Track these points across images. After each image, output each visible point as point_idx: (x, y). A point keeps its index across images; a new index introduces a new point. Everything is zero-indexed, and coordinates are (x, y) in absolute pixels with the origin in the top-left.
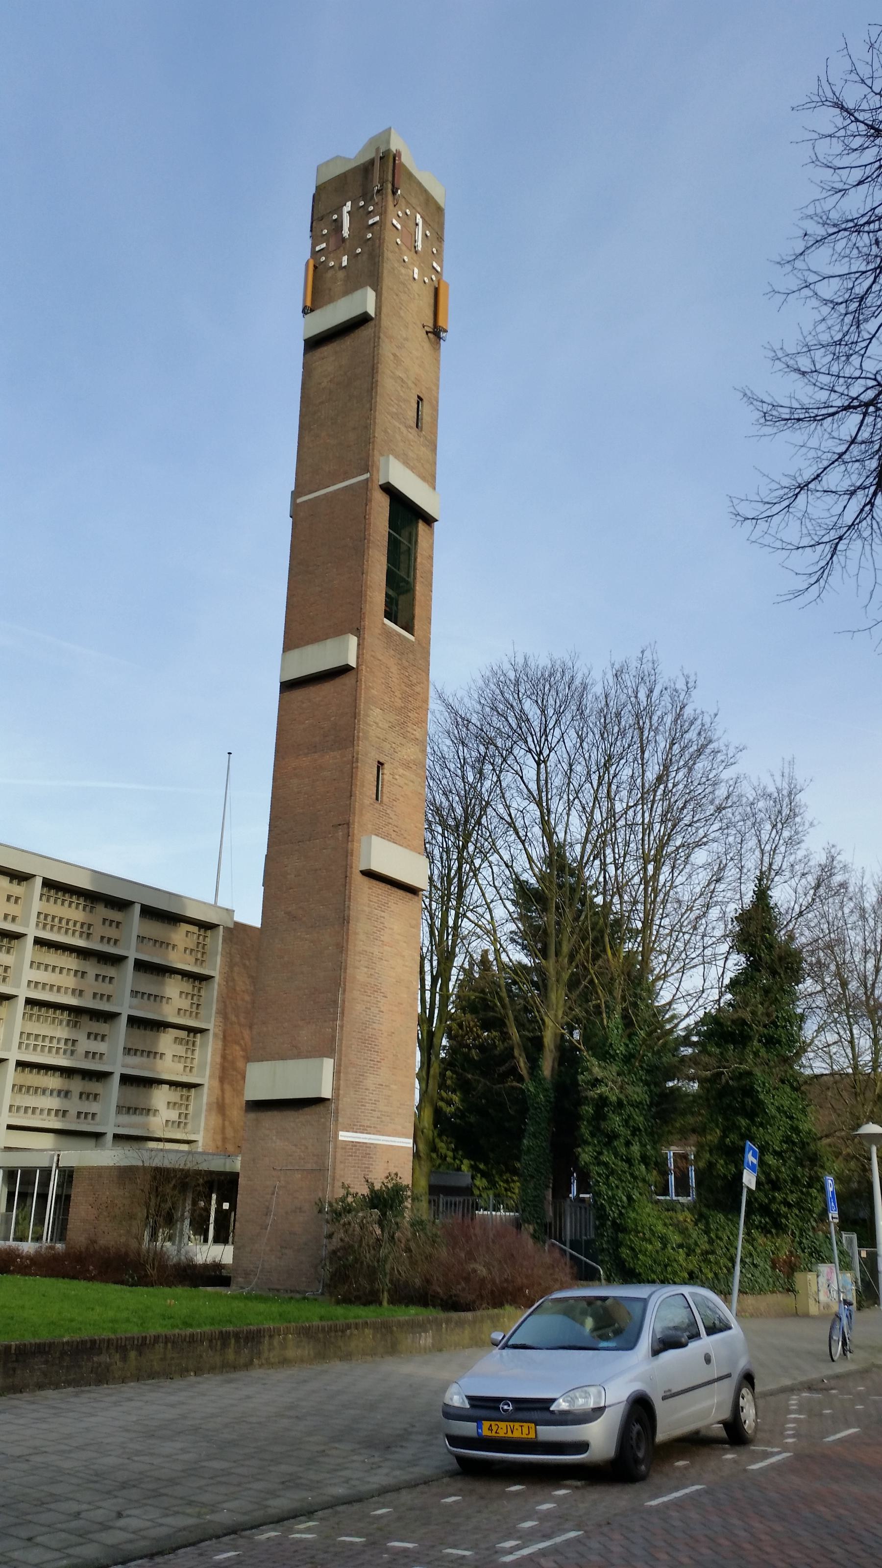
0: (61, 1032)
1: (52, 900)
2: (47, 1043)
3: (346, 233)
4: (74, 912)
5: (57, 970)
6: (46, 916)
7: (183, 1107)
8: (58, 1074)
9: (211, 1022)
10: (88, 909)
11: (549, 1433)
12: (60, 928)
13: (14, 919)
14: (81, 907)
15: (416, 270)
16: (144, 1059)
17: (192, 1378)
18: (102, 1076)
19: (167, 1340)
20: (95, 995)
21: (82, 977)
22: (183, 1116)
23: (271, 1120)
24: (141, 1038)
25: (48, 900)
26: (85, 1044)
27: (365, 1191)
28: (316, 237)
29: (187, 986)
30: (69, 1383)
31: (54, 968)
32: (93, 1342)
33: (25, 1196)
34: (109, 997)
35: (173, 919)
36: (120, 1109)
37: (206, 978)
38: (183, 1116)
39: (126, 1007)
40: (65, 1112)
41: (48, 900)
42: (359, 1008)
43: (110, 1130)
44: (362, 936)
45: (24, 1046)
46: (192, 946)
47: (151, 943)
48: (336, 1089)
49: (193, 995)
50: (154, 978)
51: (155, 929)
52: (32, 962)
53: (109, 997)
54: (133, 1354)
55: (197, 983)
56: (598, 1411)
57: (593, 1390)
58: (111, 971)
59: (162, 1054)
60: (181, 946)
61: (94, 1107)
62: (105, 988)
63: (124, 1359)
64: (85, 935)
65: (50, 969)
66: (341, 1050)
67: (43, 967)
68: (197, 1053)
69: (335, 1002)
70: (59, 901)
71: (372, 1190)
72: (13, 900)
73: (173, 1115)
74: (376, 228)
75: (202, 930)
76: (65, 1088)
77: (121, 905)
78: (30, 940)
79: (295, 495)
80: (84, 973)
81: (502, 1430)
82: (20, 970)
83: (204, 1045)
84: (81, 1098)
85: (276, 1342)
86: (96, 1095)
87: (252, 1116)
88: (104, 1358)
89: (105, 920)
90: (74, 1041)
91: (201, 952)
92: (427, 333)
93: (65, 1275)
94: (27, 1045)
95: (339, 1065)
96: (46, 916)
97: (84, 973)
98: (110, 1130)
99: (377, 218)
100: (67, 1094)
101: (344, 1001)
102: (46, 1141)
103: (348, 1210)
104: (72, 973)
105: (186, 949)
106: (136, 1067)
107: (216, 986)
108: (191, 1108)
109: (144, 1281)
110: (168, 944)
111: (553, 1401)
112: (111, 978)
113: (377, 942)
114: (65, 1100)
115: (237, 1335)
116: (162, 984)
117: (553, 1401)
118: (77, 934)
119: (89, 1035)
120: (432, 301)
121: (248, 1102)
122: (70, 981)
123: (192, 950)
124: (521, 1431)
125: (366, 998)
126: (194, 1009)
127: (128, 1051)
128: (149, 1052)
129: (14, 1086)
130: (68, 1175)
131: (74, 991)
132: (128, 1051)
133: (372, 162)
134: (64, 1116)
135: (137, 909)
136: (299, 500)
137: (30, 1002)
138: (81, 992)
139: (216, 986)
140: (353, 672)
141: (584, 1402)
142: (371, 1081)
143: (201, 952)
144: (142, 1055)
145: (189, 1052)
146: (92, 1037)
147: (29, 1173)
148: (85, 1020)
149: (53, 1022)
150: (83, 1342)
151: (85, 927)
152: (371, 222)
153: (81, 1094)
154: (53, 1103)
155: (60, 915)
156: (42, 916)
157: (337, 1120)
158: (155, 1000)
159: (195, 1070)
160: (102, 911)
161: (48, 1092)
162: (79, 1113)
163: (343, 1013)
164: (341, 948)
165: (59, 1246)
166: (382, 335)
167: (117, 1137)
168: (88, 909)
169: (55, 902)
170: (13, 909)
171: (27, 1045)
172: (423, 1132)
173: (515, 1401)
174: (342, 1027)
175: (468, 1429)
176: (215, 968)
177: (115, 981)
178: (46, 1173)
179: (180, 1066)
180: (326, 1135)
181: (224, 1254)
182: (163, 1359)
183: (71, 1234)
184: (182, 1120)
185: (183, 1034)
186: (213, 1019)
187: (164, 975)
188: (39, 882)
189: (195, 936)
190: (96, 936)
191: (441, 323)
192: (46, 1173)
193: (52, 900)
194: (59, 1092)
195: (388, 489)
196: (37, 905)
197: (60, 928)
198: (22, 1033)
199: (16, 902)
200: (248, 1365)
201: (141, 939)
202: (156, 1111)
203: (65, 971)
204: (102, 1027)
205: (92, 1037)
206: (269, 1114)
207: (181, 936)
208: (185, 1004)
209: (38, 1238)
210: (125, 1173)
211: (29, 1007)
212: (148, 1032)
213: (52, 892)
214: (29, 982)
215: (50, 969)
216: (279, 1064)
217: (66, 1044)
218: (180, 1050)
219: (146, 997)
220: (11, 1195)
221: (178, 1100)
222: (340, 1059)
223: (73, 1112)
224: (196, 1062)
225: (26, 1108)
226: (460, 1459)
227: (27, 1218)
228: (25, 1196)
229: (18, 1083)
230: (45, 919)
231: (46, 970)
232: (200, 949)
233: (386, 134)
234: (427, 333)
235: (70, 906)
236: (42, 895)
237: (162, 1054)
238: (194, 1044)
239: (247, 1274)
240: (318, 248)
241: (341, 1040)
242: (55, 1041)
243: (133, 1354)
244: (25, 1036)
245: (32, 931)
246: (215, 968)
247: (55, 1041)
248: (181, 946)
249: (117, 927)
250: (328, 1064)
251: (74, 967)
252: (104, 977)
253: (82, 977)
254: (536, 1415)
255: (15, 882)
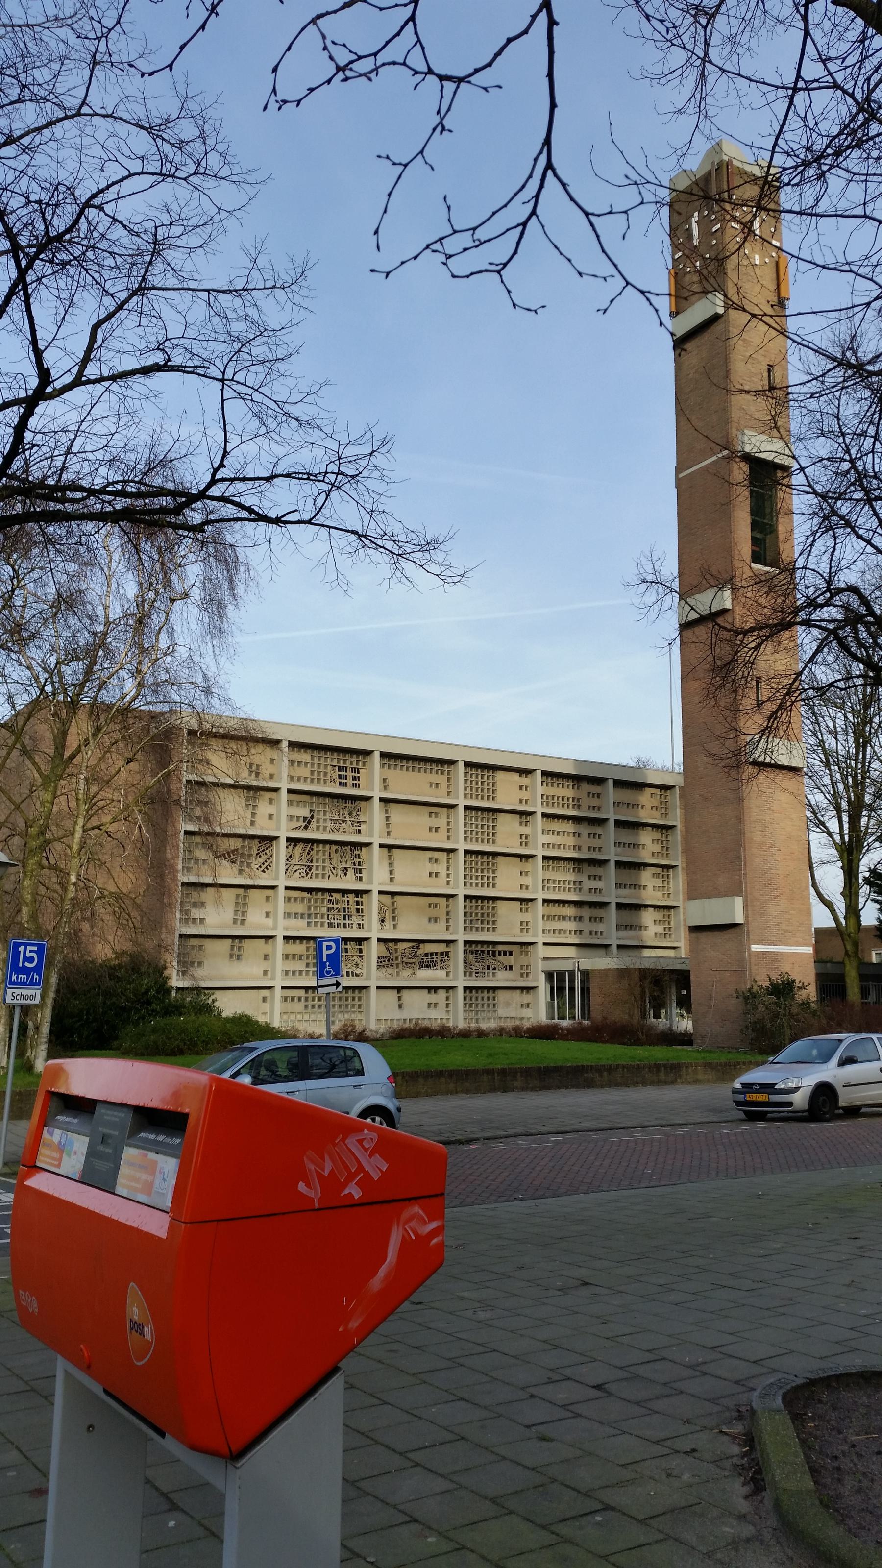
0: (570, 877)
1: (550, 784)
2: (562, 885)
3: (696, 242)
4: (566, 791)
5: (561, 833)
6: (548, 796)
7: (667, 923)
8: (572, 905)
9: (678, 860)
10: (576, 787)
11: (775, 1098)
12: (558, 803)
13: (526, 802)
14: (571, 787)
15: (757, 257)
16: (632, 891)
17: (640, 1087)
18: (604, 905)
19: (624, 1067)
20: (590, 848)
21: (579, 836)
22: (667, 930)
23: (704, 937)
24: (627, 876)
25: (547, 785)
26: (588, 884)
27: (767, 984)
28: (675, 247)
29: (657, 835)
30: (573, 1087)
31: (559, 832)
32: (583, 1066)
33: (561, 989)
34: (600, 849)
35: (640, 786)
36: (619, 927)
37: (671, 827)
38: (667, 930)
39: (612, 855)
40: (581, 931)
41: (547, 785)
42: (757, 860)
43: (615, 942)
44: (755, 810)
45: (546, 889)
46: (657, 804)
47: (625, 805)
48: (746, 917)
49: (662, 841)
50: (630, 831)
51: (626, 795)
52: (543, 831)
53: (600, 849)
54: (605, 1073)
55: (664, 831)
56: (797, 1089)
57: (796, 1080)
58: (598, 830)
59: (645, 886)
60: (648, 806)
61: (600, 927)
62: (596, 843)
63: (601, 1076)
64: (576, 807)
65: (556, 833)
66: (746, 891)
67: (551, 833)
68: (671, 883)
69: (739, 857)
70: (555, 785)
71: (772, 984)
72: (524, 788)
73: (660, 929)
74: (719, 234)
75: (663, 791)
76: (579, 915)
77: (599, 781)
78: (539, 816)
79: (678, 470)
80: (579, 834)
81: (754, 1097)
82: (535, 837)
83: (676, 877)
84: (590, 920)
85: (690, 1070)
86: (601, 919)
87: (694, 935)
88: (590, 1075)
89: (589, 794)
90: (580, 882)
91: (664, 808)
92: (772, 306)
93: (590, 1040)
94: (549, 888)
95: (746, 901)
96: (548, 796)
97: (579, 834)
98: (615, 942)
99: (718, 226)
100: (580, 919)
101: (745, 856)
102: (571, 952)
103: (754, 996)
104: (572, 835)
105: (652, 807)
106: (627, 896)
107: (679, 832)
108: (672, 923)
109: (638, 1042)
110: (638, 805)
111: (776, 1084)
112: (600, 835)
113: (768, 812)
114: (580, 923)
115: (665, 1066)
116: (637, 834)
117: (776, 1084)
118: (571, 806)
119: (590, 876)
120: (775, 275)
121: (690, 927)
122: (570, 841)
123: (657, 808)
124: (762, 1098)
125: (762, 853)
126: (665, 851)
127: (619, 886)
128: (635, 886)
129: (543, 916)
130: (586, 975)
131: (574, 847)
132: (619, 886)
133: (710, 173)
134: (580, 934)
135: (611, 782)
136: (681, 476)
137: (545, 858)
138: (580, 847)
139: (679, 832)
140: (730, 612)
141: (791, 1085)
142: (773, 910)
143: (664, 808)
144: (630, 888)
145: (666, 883)
146: (592, 878)
147: (561, 974)
148: (585, 866)
149: (564, 870)
150: (578, 1066)
151: (576, 800)
152: (714, 229)
153: (590, 918)
154: (571, 925)
155: (557, 795)
156: (545, 797)
157: (749, 938)
158: (634, 847)
159: (671, 896)
160: (586, 787)
161: (567, 918)
162: (591, 932)
163: (745, 865)
164: (740, 819)
165: (586, 1022)
166: (731, 329)
167: (620, 947)
168: (576, 787)
169: (552, 786)
170: (525, 795)
171: (549, 888)
172: (849, 936)
173: (759, 1084)
174: (745, 874)
175: (741, 1097)
176: (676, 819)
177: (602, 837)
178: (572, 974)
179: (660, 894)
180: (742, 948)
181: (686, 1025)
182: (622, 1077)
183: (593, 1014)
184: (667, 932)
185: (659, 870)
186: (680, 858)
187: (638, 829)
188: (539, 773)
189: (658, 796)
190: (584, 807)
191: (783, 295)
192: (572, 974)
193: (550, 784)
194: (575, 918)
195: (747, 458)
196: (540, 790)
197: (558, 803)
198: (543, 880)
199: (526, 790)
200: (673, 1082)
201: (617, 804)
202: (646, 927)
203: (566, 834)
204: (598, 871)
205: (592, 878)
206: (704, 934)
207: (646, 798)
208: (657, 848)
209: (573, 1017)
210: (623, 973)
211: (545, 861)
212: (632, 871)
213: (549, 779)
214: (543, 844)
215: (556, 833)
216: (706, 902)
217: (574, 884)
218: (659, 882)
219: (627, 845)
220: (552, 989)
221: (661, 918)
222: (746, 897)
223: (586, 931)
224: (671, 890)
225: (554, 930)
226: (745, 1112)
227: (564, 1004)
228: (561, 989)
229: (547, 913)
230: (548, 798)
231: (553, 834)
232: (663, 805)
233: (718, 147)
234: (772, 306)
235: (563, 787)
236: (542, 782)
237: (645, 886)
238: (668, 876)
239: (703, 1037)
240: (676, 257)
241: (746, 883)
242: (567, 883)
243: (605, 1073)
244: (546, 882)
245: (540, 809)
246: (676, 819)
247: (567, 883)
248: (648, 806)
249: (598, 797)
250: (739, 901)
251: (572, 831)
252: (594, 835)
253: (579, 836)
254: (768, 1090)
255: (523, 775)
